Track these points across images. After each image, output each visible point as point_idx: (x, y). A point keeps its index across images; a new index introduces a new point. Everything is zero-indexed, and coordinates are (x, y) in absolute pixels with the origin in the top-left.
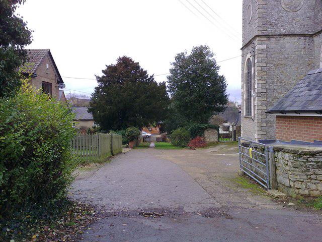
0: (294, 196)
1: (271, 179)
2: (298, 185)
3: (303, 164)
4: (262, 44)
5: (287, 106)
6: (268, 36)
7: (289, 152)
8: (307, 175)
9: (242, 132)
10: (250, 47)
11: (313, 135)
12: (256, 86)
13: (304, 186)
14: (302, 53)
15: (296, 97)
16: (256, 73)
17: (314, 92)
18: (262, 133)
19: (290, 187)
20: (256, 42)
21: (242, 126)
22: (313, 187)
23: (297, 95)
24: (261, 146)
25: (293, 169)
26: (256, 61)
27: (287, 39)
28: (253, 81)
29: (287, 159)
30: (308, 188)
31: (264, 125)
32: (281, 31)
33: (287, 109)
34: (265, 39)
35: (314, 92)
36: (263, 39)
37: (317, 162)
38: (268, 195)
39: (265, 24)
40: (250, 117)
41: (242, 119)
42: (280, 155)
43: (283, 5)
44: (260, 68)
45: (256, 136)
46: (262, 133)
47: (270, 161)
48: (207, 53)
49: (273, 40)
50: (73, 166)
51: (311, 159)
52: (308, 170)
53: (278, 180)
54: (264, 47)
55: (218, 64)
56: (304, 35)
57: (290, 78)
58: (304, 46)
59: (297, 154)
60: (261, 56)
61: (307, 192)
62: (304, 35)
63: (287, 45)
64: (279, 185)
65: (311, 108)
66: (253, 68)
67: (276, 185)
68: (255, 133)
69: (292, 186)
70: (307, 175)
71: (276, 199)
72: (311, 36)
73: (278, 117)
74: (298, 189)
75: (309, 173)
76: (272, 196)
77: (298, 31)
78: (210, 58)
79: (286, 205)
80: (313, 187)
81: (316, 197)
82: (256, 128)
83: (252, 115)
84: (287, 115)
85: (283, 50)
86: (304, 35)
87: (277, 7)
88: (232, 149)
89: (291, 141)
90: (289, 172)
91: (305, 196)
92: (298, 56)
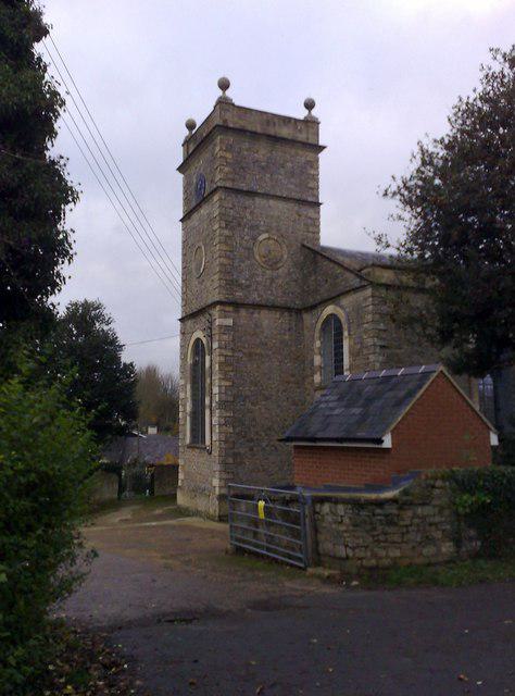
0: (354, 571)
1: (310, 549)
2: (360, 553)
3: (367, 519)
4: (225, 317)
5: (314, 427)
6: (237, 305)
7: (344, 501)
8: (373, 536)
9: (181, 476)
10: (203, 319)
11: (363, 475)
12: (216, 390)
13: (369, 554)
14: (287, 337)
15: (328, 416)
16: (217, 368)
17: (356, 411)
18: (224, 476)
19: (347, 558)
20: (216, 312)
21: (181, 462)
22: (383, 553)
23: (327, 413)
24: (282, 495)
25: (351, 528)
26: (215, 345)
27: (264, 313)
28: (208, 381)
29: (343, 514)
30: (375, 556)
31: (231, 460)
32: (255, 297)
33: (319, 435)
34: (231, 309)
35: (356, 411)
36: (227, 309)
37: (386, 516)
38: (312, 576)
39: (230, 283)
40: (200, 445)
41: (181, 449)
42: (326, 508)
43: (257, 257)
44: (222, 359)
45: (216, 482)
46: (224, 476)
47: (307, 520)
48: (99, 317)
49: (243, 312)
50: (73, 514)
51: (378, 511)
52: (374, 529)
53: (320, 549)
54: (229, 322)
55: (122, 340)
56: (289, 309)
57: (269, 379)
58: (288, 326)
59: (358, 505)
60: (225, 337)
61: (373, 562)
62: (289, 309)
63: (265, 323)
64: (322, 559)
65: (360, 434)
66: (207, 358)
67: (318, 559)
68: (213, 476)
69: (351, 555)
70: (373, 536)
71: (329, 580)
72: (299, 311)
73: (296, 447)
74: (359, 559)
75: (376, 533)
76: (319, 577)
77: (280, 301)
78: (106, 328)
79: (348, 586)
80: (383, 553)
81: (387, 568)
82: (217, 467)
83: (208, 442)
84: (345, 445)
85: (257, 330)
86: (289, 308)
87: (248, 259)
88: (158, 511)
89: (325, 486)
90: (345, 535)
91: (371, 569)
92: (281, 343)
